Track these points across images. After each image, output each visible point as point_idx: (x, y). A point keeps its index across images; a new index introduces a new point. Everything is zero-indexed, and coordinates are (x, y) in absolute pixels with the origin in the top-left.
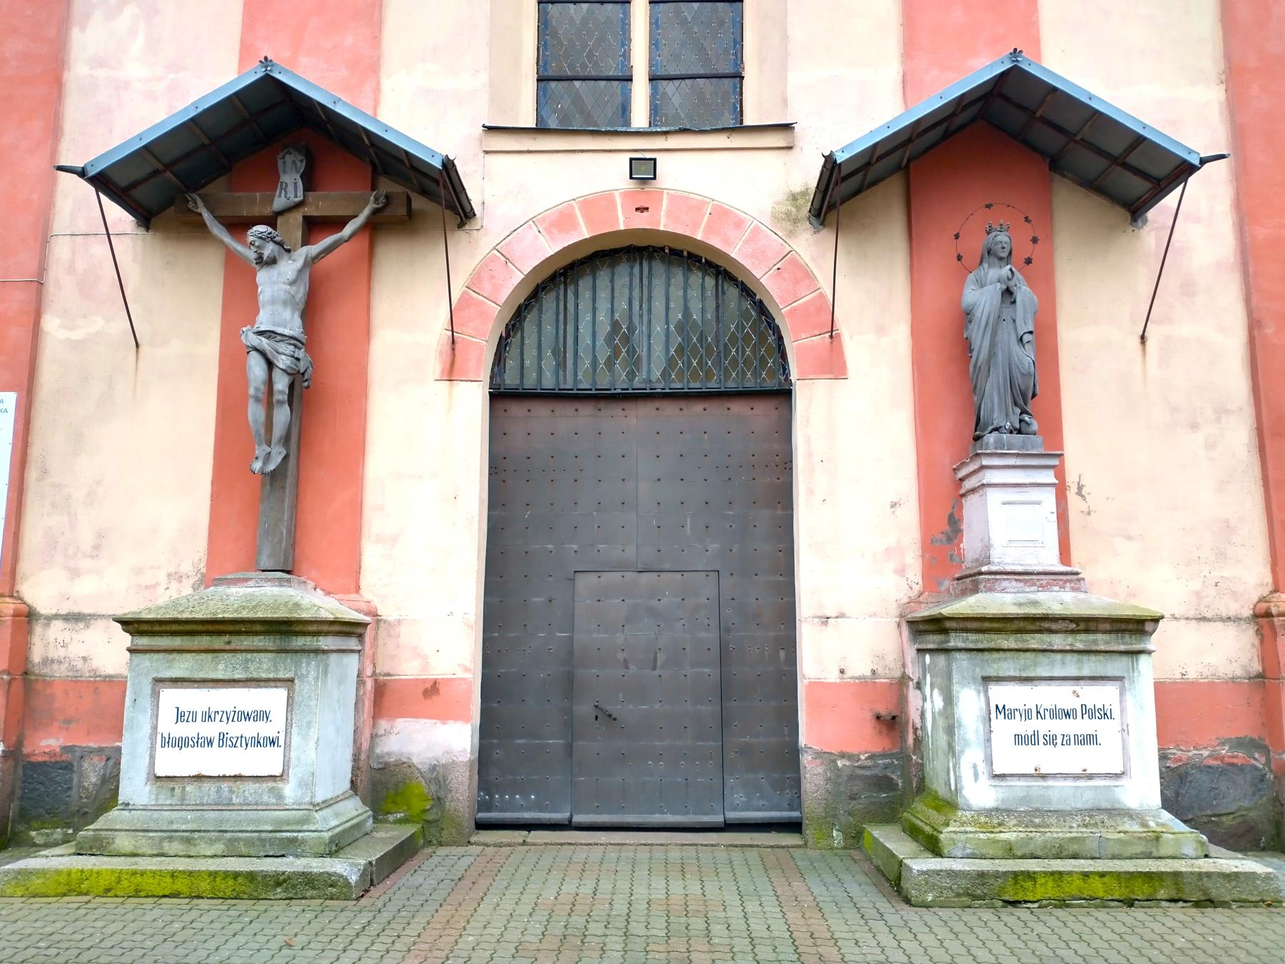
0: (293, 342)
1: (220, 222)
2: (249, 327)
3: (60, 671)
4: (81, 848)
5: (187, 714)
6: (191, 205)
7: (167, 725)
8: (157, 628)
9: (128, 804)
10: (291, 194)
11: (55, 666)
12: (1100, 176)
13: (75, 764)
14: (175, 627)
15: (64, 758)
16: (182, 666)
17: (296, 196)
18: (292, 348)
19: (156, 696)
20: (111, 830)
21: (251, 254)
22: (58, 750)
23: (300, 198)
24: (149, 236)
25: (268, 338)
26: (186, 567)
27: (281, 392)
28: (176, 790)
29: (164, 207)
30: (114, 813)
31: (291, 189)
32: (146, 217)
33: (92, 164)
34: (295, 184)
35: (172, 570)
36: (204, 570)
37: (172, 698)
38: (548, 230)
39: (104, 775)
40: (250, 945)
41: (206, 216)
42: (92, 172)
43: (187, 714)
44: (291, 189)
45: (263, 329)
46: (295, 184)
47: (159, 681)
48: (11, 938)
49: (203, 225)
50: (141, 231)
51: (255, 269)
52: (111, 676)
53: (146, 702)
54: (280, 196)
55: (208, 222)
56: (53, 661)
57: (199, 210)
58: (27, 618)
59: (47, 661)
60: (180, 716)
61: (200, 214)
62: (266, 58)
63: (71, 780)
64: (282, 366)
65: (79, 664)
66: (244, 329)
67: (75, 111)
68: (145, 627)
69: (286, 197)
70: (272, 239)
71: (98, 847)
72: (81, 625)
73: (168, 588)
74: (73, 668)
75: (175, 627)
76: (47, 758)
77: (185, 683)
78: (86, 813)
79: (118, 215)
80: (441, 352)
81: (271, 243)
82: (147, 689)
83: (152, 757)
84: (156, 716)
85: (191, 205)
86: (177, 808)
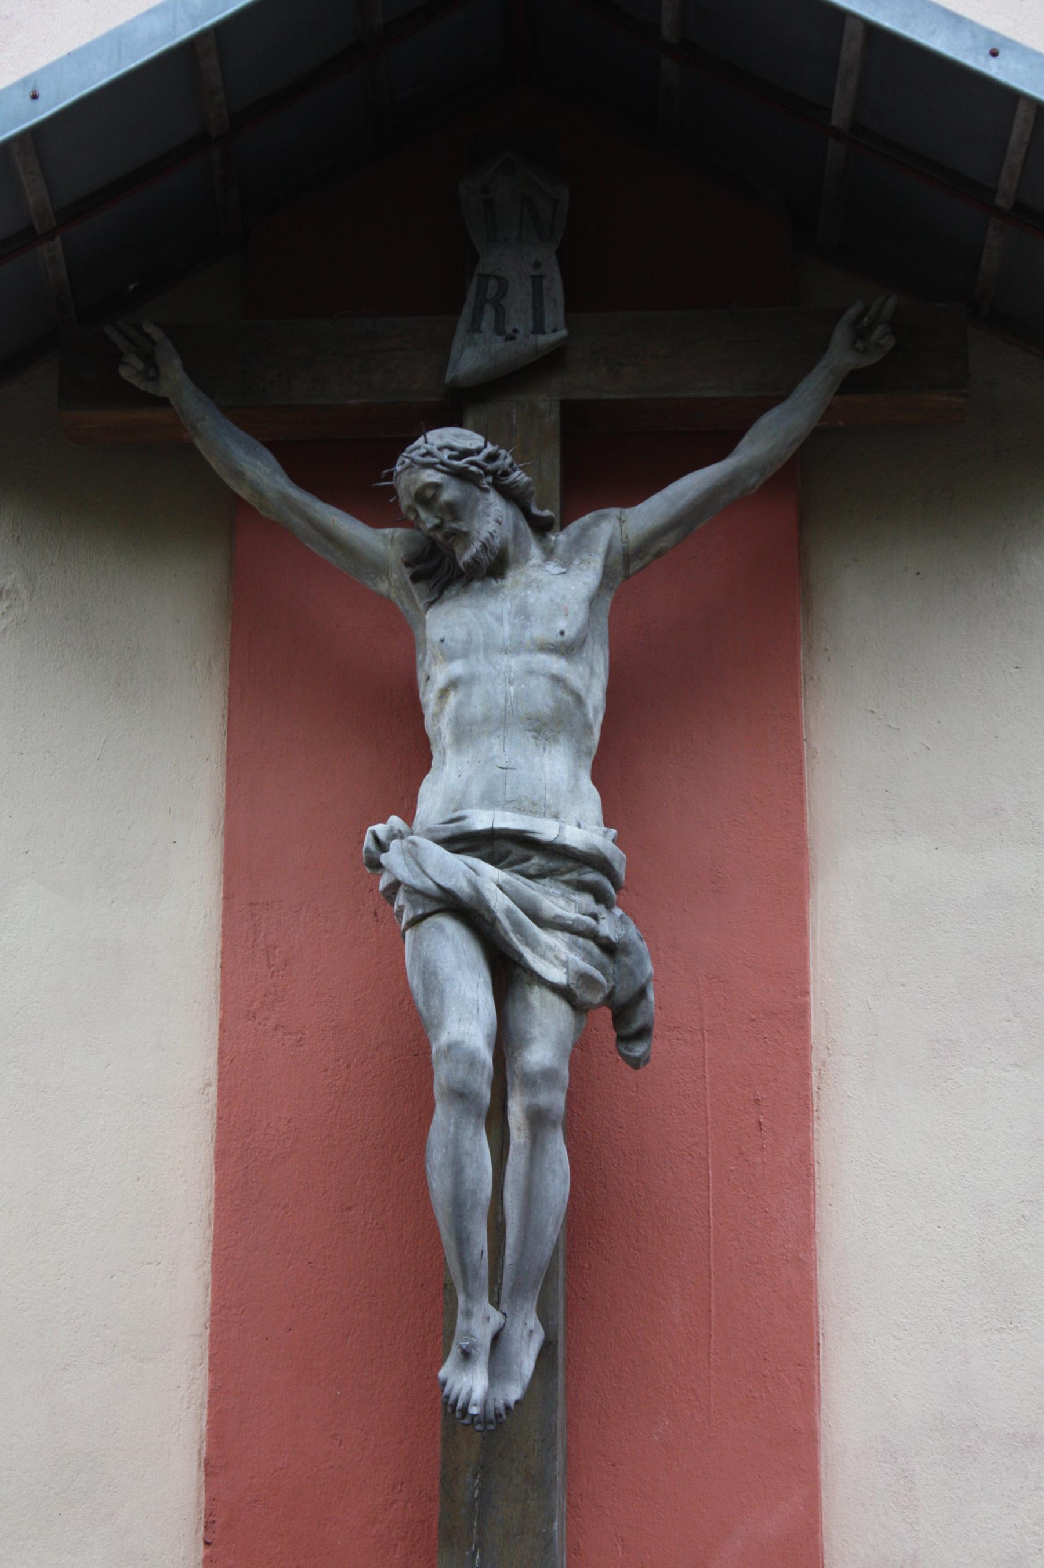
0: (591, 876)
6: (130, 372)
10: (519, 319)
12: (539, 833)
17: (539, 329)
18: (586, 900)
23: (554, 335)
25: (495, 861)
27: (548, 1076)
31: (519, 298)
34: (537, 282)
38: (567, 653)
44: (519, 298)
46: (537, 282)
51: (404, 606)
57: (164, 389)
64: (557, 975)
66: (380, 829)
80: (488, 1035)
85: (130, 372)
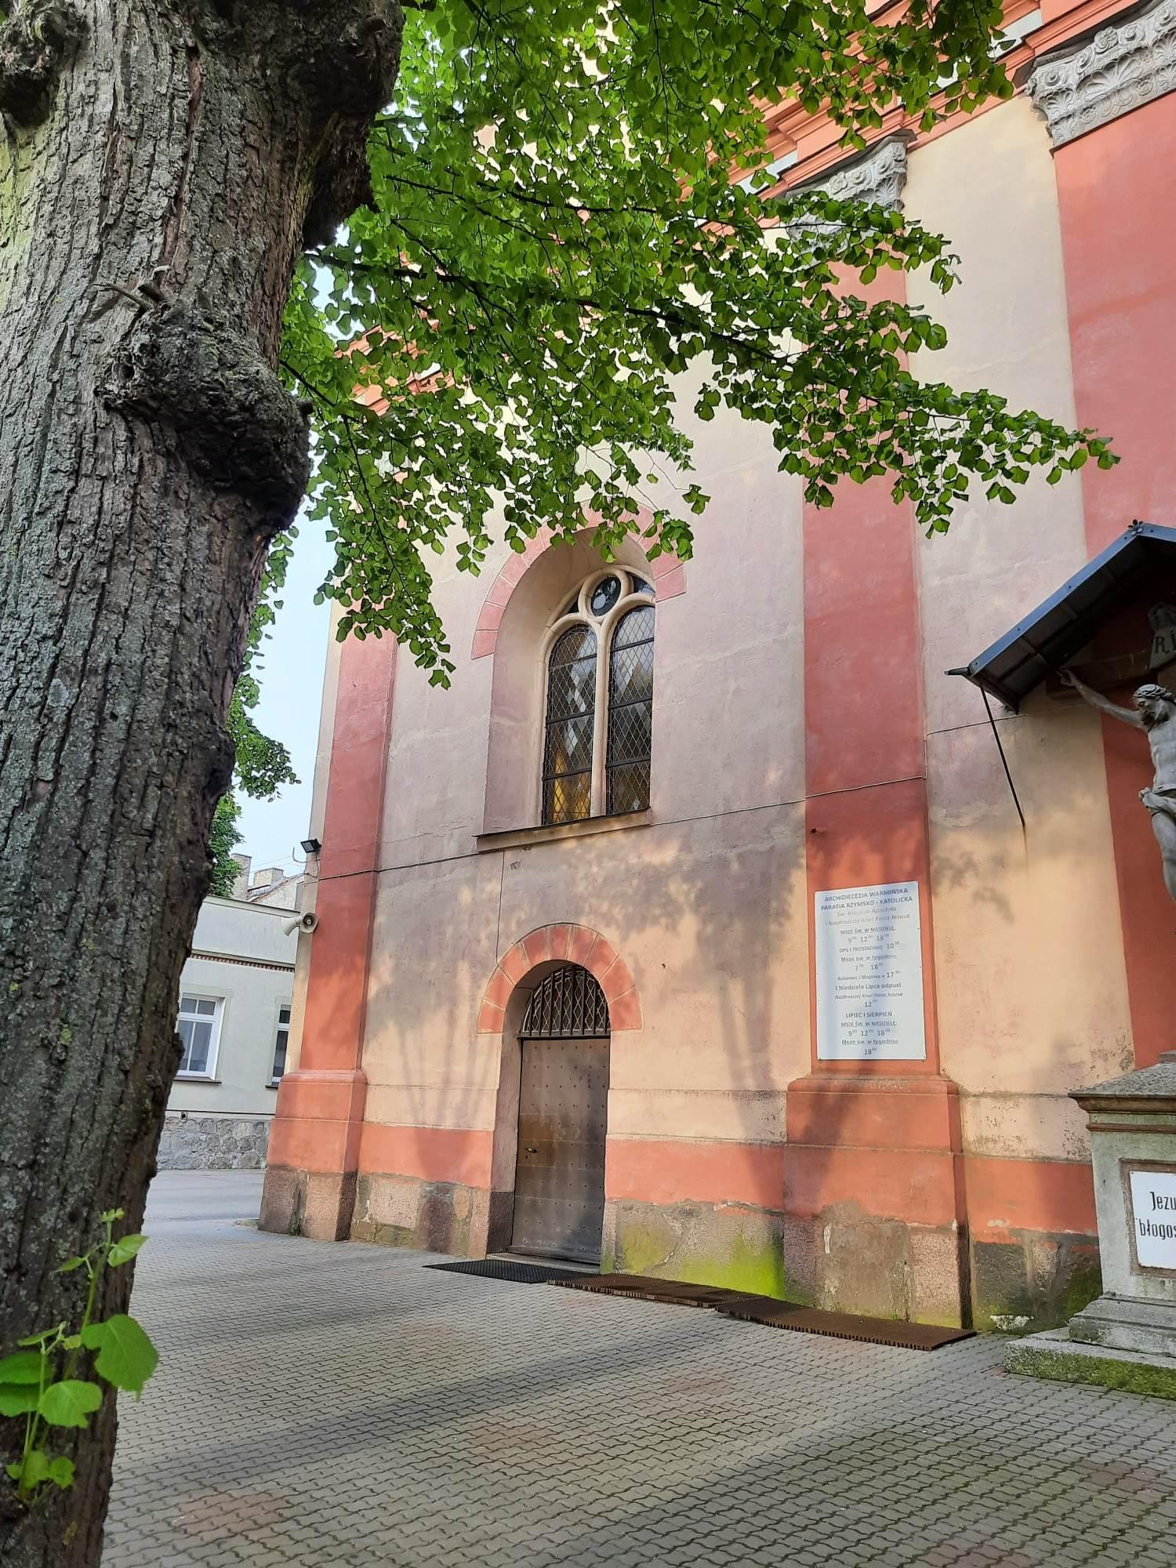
1: (1097, 691)
2: (1147, 789)
3: (995, 1150)
4: (1076, 1336)
5: (1164, 1200)
7: (1143, 1210)
8: (1115, 1105)
9: (1114, 1294)
11: (990, 1145)
13: (1026, 1248)
14: (1135, 1105)
15: (1014, 1240)
16: (1147, 1148)
19: (1126, 1179)
20: (1105, 1320)
21: (1137, 715)
22: (1006, 1232)
24: (1019, 719)
26: (1109, 1045)
28: (1167, 1284)
29: (1030, 687)
30: (1101, 1302)
32: (1014, 701)
33: (975, 662)
35: (1094, 1047)
36: (1132, 1048)
37: (1141, 1180)
39: (1058, 1263)
40: (921, 1478)
41: (1080, 687)
42: (977, 669)
43: (1164, 1200)
45: (1167, 787)
47: (1124, 1162)
48: (662, 1425)
49: (1079, 696)
50: (1011, 715)
52: (1048, 1158)
53: (1116, 1183)
54: (1157, 651)
55: (1084, 693)
56: (987, 1140)
57: (1072, 684)
58: (955, 1094)
59: (981, 1140)
60: (1156, 1202)
61: (1074, 687)
62: (1135, 522)
63: (1023, 1265)
65: (1015, 1144)
66: (1143, 792)
67: (933, 618)
68: (1103, 1104)
69: (1163, 651)
70: (1162, 697)
71: (1090, 1336)
72: (1011, 1104)
73: (1094, 1067)
74: (1008, 1148)
75: (1135, 1105)
76: (996, 1240)
77: (1157, 1167)
78: (1045, 1303)
79: (995, 703)
81: (1161, 701)
82: (1116, 1172)
83: (1133, 1245)
84: (1129, 1200)
86: (1171, 1304)
